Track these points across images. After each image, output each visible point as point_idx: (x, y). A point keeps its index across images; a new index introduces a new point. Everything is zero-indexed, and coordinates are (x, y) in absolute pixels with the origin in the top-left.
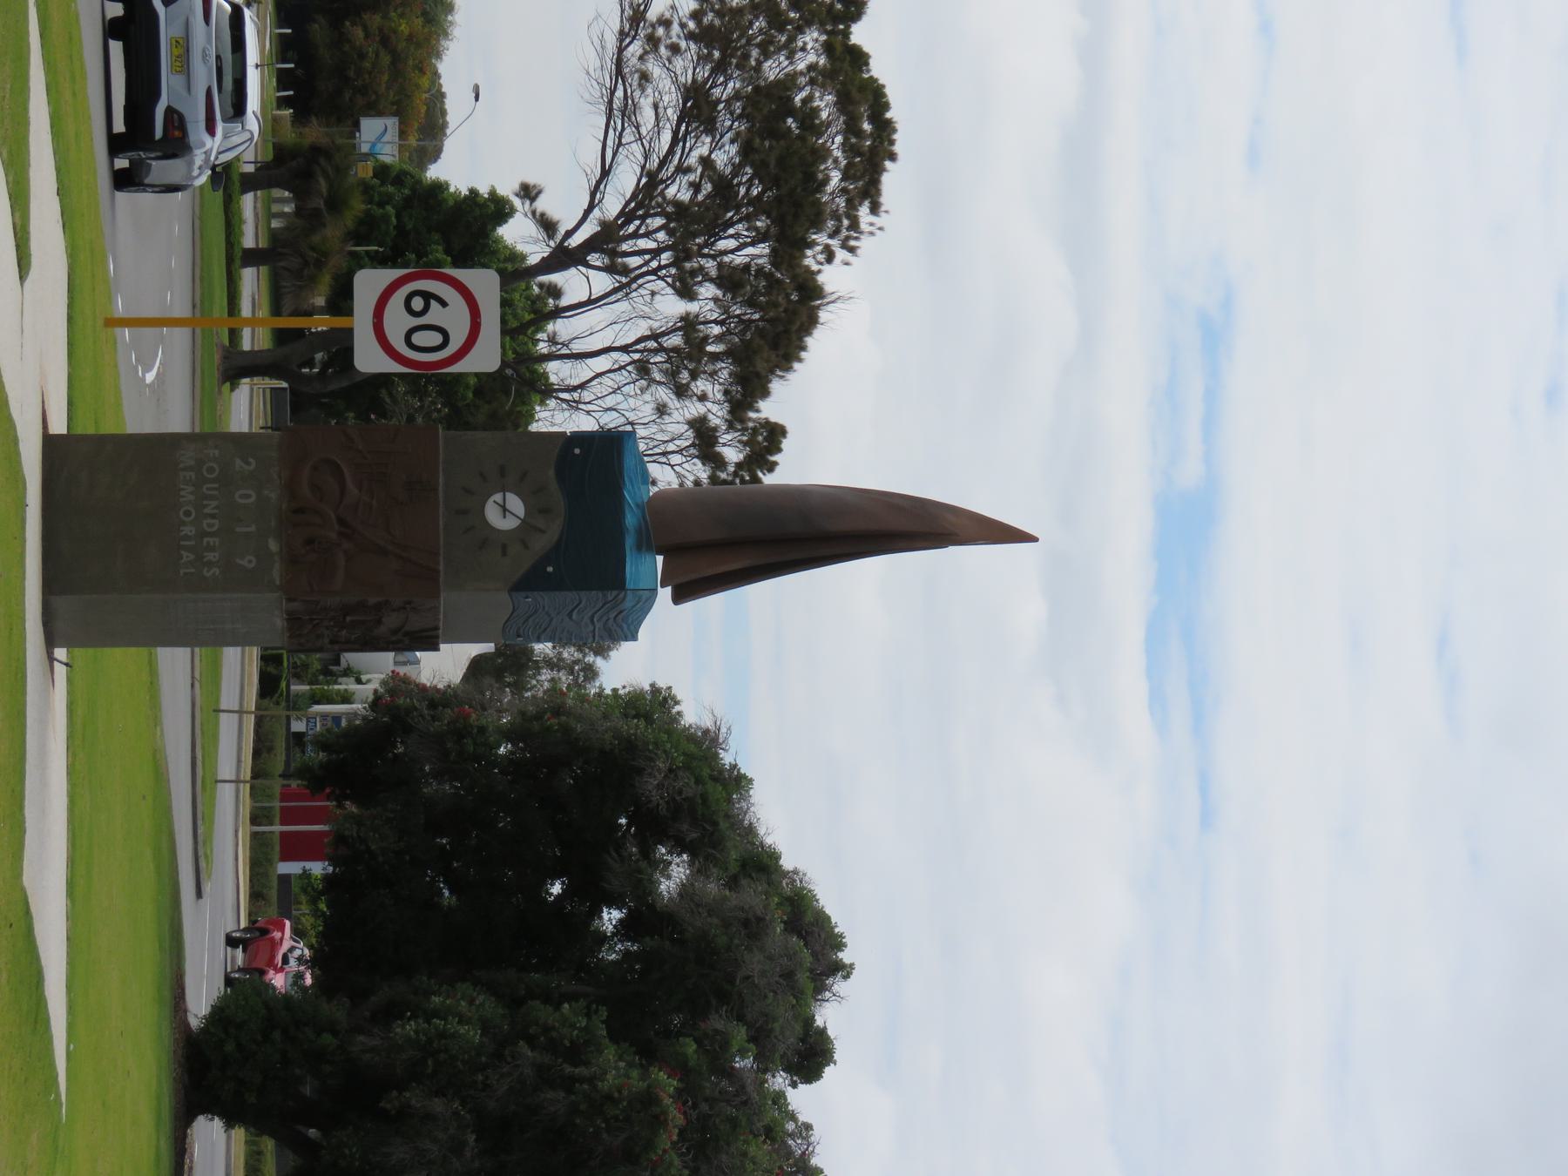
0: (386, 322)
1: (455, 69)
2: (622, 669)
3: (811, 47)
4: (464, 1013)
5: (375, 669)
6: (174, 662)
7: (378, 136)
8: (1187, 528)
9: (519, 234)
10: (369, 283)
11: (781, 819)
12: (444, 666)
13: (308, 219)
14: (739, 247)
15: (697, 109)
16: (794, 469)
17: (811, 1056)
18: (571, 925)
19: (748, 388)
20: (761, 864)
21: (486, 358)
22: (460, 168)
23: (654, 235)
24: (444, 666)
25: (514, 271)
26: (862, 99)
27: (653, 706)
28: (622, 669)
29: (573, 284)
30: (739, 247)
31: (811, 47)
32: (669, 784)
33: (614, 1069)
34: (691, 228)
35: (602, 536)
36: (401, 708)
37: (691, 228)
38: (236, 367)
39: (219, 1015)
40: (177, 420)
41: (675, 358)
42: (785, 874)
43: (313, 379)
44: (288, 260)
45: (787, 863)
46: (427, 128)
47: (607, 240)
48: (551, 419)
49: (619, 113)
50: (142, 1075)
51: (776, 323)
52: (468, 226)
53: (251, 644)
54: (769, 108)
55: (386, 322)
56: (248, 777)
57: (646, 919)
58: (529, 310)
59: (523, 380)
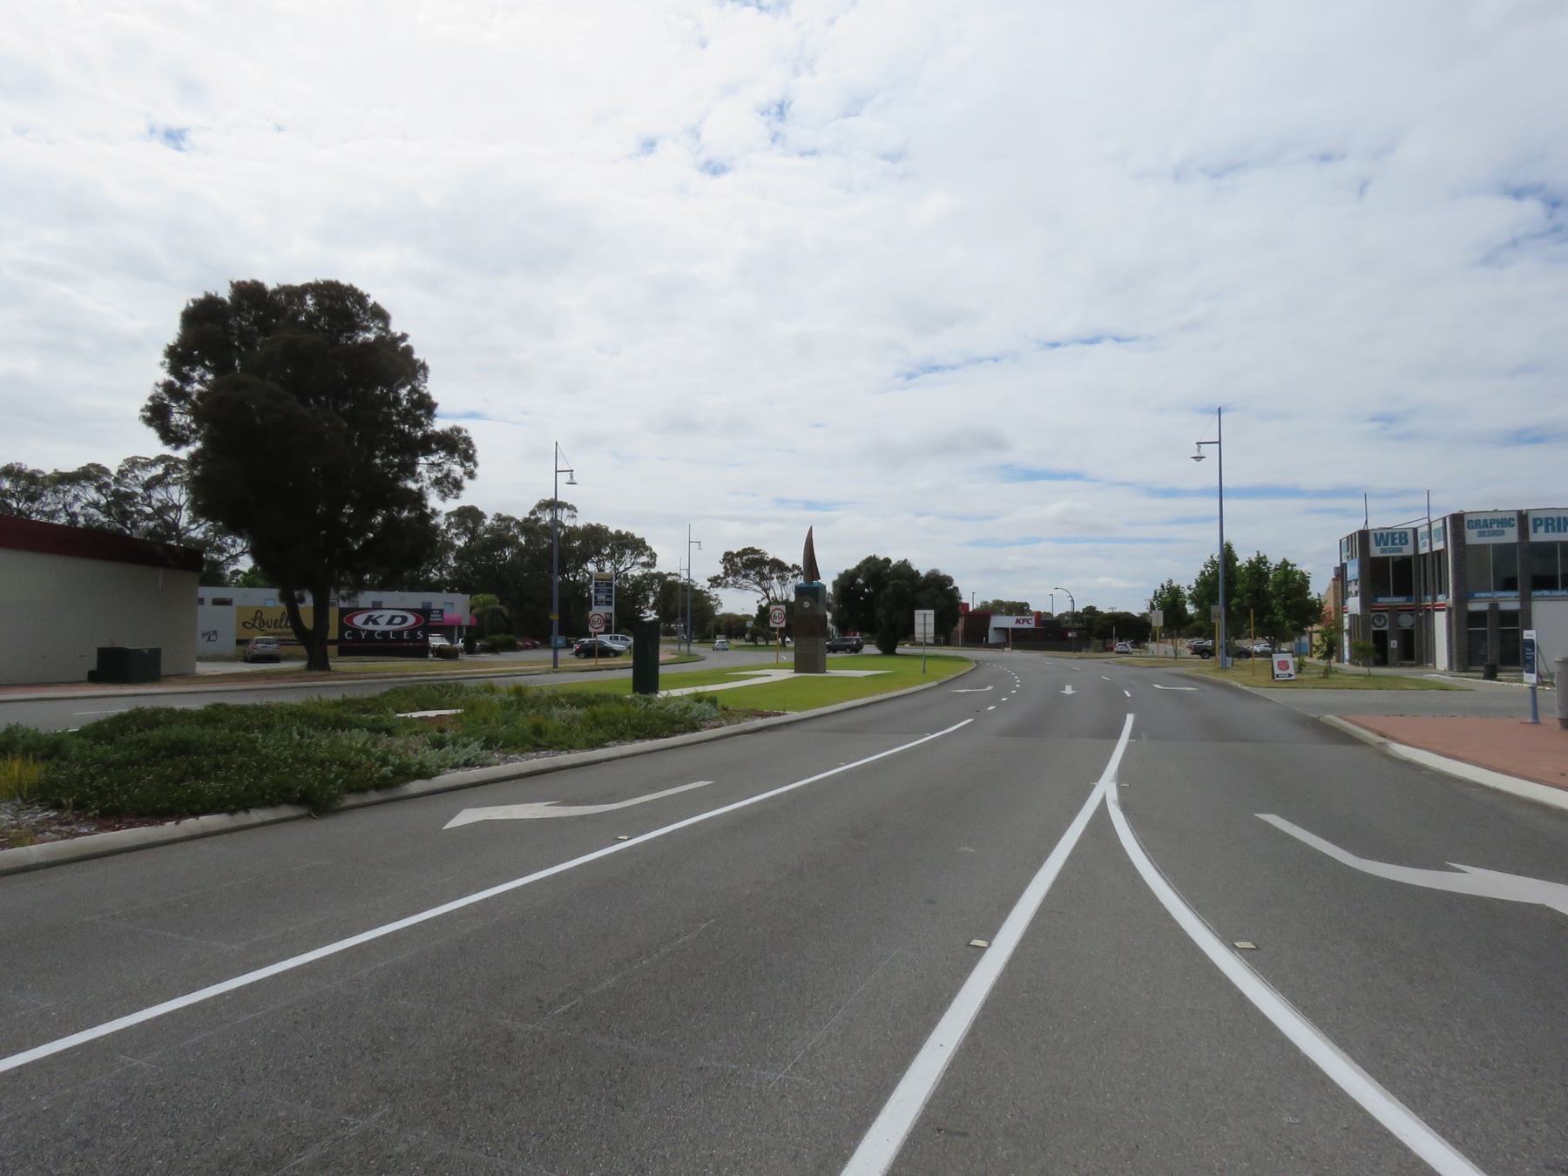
0: (778, 622)
1: (740, 613)
2: (829, 589)
3: (737, 560)
4: (880, 612)
5: (830, 625)
6: (662, 670)
7: (749, 624)
8: (810, 505)
9: (764, 604)
10: (772, 625)
11: (852, 565)
12: (829, 616)
13: (762, 635)
14: (766, 570)
15: (746, 576)
16: (800, 562)
17: (888, 561)
18: (867, 596)
19: (787, 569)
20: (859, 568)
21: (783, 607)
22: (754, 612)
23: (765, 583)
24: (829, 616)
25: (770, 604)
26: (745, 552)
27: (835, 584)
28: (829, 589)
29: (772, 595)
30: (766, 570)
31: (737, 560)
32: (847, 582)
33: (889, 590)
34: (763, 577)
35: (810, 592)
36: (834, 621)
37: (763, 577)
38: (784, 644)
39: (880, 647)
40: (792, 654)
41: (782, 579)
42: (275, 292)
43: (785, 632)
44: (768, 638)
45: (271, 285)
46: (748, 617)
47: (765, 590)
48: (792, 598)
49: (746, 588)
50: (889, 660)
51: (778, 565)
52: (764, 613)
53: (325, 652)
54: (747, 566)
55: (778, 622)
56: (549, 654)
57: (867, 585)
58: (776, 602)
59: (786, 603)
